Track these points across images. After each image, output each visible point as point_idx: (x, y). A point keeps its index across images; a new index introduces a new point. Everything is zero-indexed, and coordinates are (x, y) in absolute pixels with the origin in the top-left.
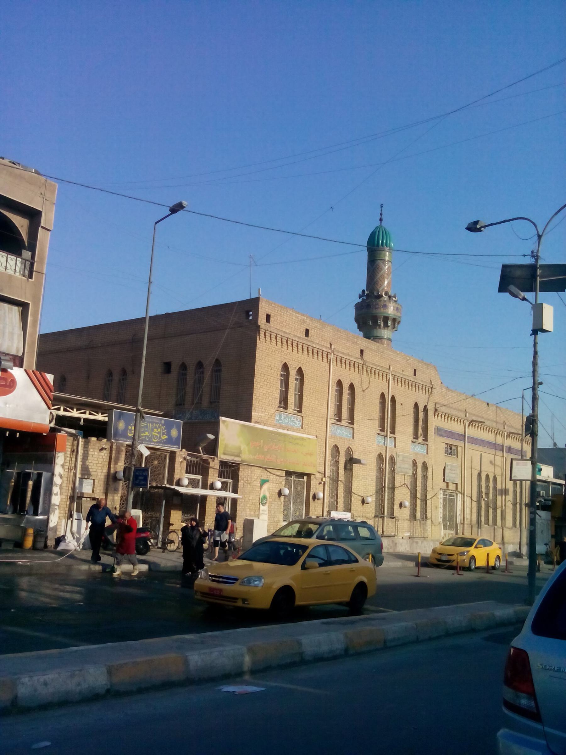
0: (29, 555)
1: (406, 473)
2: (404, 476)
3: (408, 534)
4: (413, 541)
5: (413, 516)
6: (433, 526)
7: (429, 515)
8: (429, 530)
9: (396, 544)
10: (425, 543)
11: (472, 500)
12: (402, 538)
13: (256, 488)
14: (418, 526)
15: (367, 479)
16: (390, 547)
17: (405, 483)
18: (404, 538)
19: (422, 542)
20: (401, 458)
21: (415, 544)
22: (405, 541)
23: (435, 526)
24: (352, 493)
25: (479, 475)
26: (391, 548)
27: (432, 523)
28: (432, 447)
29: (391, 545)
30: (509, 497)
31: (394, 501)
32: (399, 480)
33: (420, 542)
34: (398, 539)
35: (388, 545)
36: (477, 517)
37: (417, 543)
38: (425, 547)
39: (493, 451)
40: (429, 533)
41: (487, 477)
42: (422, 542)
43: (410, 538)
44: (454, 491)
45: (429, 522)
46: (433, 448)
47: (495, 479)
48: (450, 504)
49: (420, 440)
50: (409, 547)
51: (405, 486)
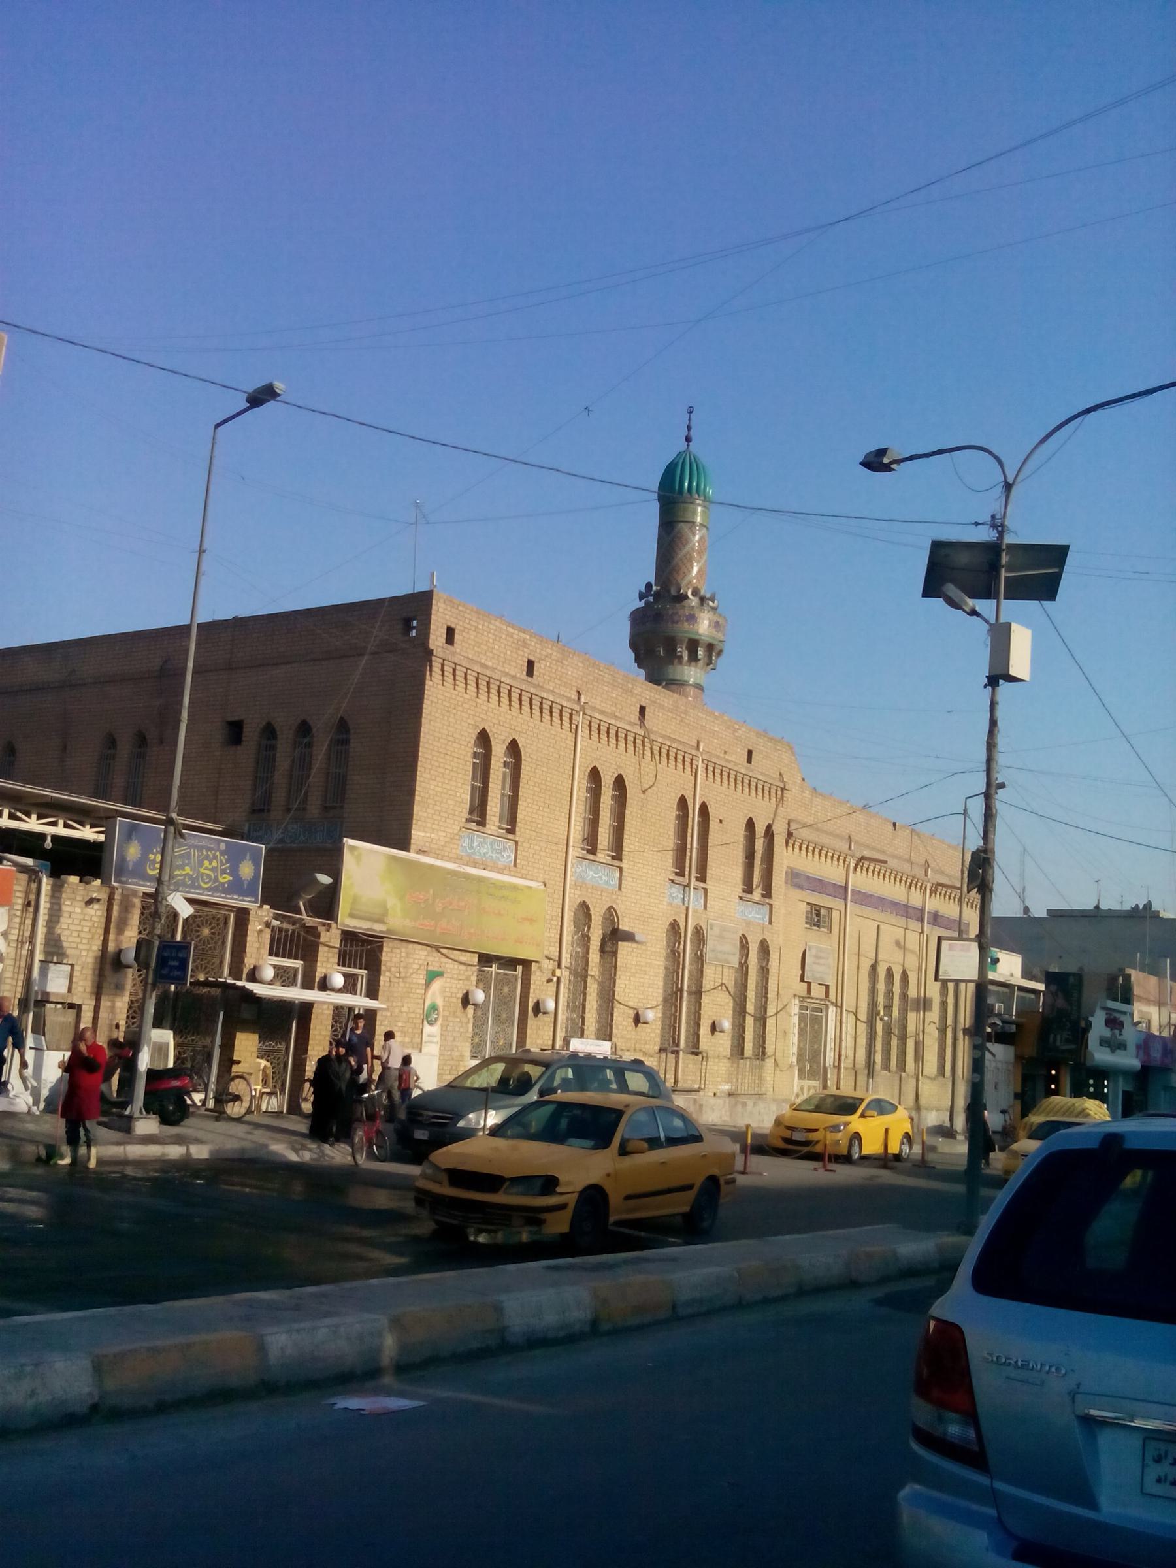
2: (721, 969)
3: (727, 1087)
5: (738, 1050)
6: (777, 1072)
8: (768, 1079)
9: (701, 1106)
12: (715, 1094)
14: (748, 1070)
17: (724, 982)
18: (718, 1094)
19: (755, 1104)
20: (716, 931)
21: (739, 1107)
25: (874, 968)
27: (776, 1064)
32: (711, 976)
33: (750, 1104)
34: (706, 1097)
37: (744, 1104)
39: (902, 921)
40: (769, 1086)
41: (890, 973)
42: (755, 1104)
45: (769, 1063)
49: (757, 894)
50: (728, 1113)
51: (724, 989)
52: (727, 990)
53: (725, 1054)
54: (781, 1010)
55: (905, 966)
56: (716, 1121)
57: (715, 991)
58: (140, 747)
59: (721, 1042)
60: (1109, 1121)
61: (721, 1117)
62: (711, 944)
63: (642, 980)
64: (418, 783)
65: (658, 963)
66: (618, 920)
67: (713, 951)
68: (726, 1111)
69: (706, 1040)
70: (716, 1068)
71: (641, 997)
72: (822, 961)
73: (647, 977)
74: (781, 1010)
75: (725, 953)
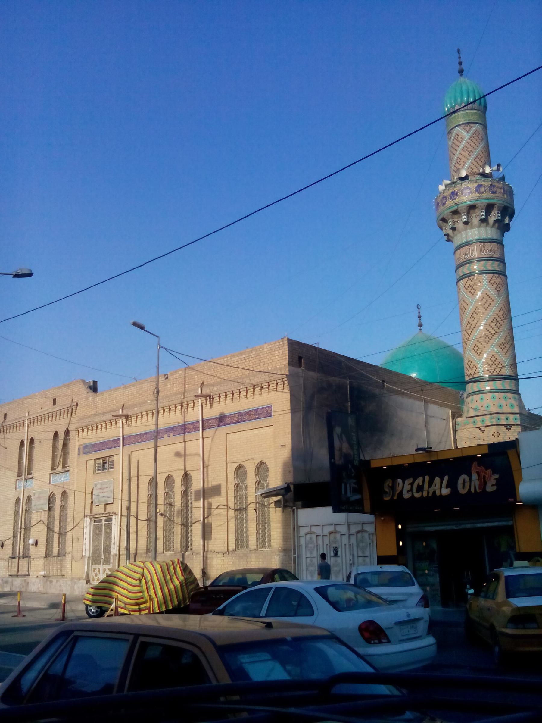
0: (469, 203)
1: (42, 509)
2: (40, 513)
3: (42, 573)
4: (47, 581)
5: (48, 554)
6: (74, 562)
7: (68, 549)
8: (68, 566)
9: (28, 583)
10: (61, 582)
11: (73, 529)
12: (37, 577)
13: (136, 399)
14: (55, 563)
15: (6, 525)
16: (22, 587)
17: (42, 519)
18: (39, 577)
19: (57, 581)
20: (37, 495)
21: (48, 583)
22: (38, 580)
23: (76, 561)
24: (136, 517)
25: (153, 483)
26: (23, 587)
27: (73, 558)
28: (74, 470)
29: (24, 584)
30: (221, 499)
31: (47, 540)
32: (35, 517)
33: (54, 581)
34: (32, 578)
35: (21, 585)
36: (299, 531)
37: (51, 582)
38: (60, 586)
39: (180, 438)
40: (68, 570)
41: (169, 480)
42: (57, 581)
43: (45, 577)
44: (103, 514)
45: (68, 557)
46: (76, 471)
47: (186, 477)
48: (105, 531)
49: (60, 469)
50: (42, 586)
51: (42, 522)
52: (44, 523)
53: (42, 555)
54: (75, 527)
55: (187, 469)
56: (35, 590)
57: (38, 525)
58: (18, 476)
59: (40, 550)
60: (248, 573)
61: (38, 588)
62: (34, 502)
63: (4, 528)
64: (289, 399)
65: (11, 519)
66: (164, 483)
67: (35, 506)
68: (40, 585)
69: (32, 550)
70: (38, 563)
71: (4, 535)
72: (105, 490)
73: (7, 526)
74: (75, 527)
75: (41, 505)
